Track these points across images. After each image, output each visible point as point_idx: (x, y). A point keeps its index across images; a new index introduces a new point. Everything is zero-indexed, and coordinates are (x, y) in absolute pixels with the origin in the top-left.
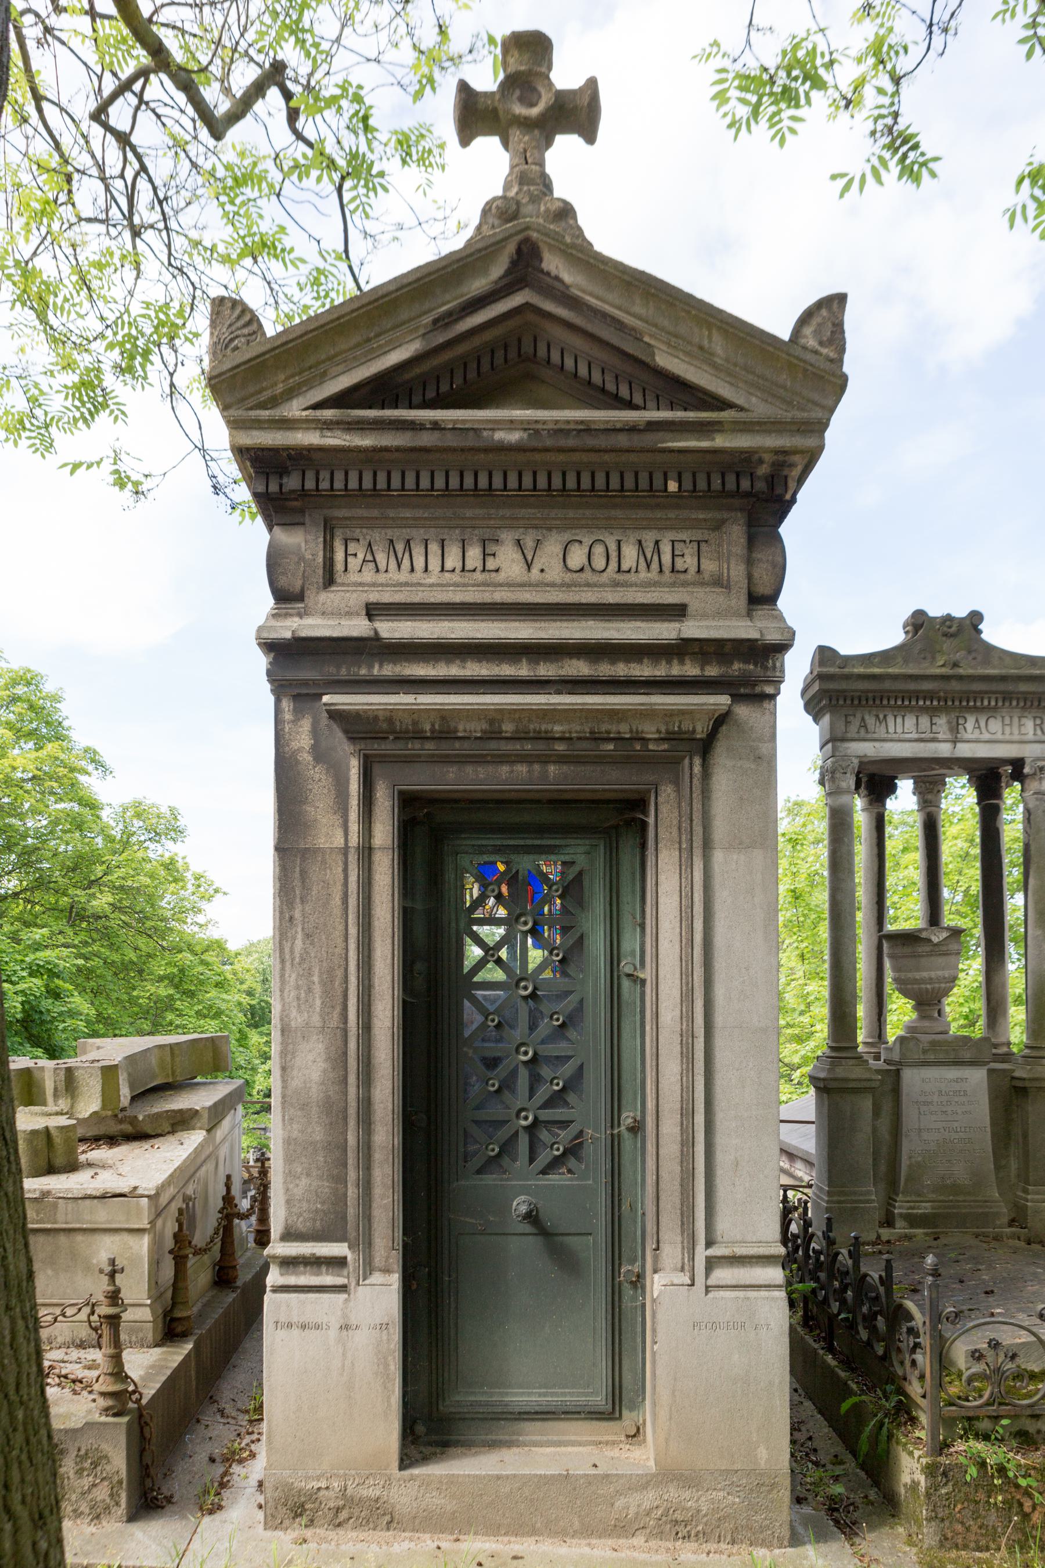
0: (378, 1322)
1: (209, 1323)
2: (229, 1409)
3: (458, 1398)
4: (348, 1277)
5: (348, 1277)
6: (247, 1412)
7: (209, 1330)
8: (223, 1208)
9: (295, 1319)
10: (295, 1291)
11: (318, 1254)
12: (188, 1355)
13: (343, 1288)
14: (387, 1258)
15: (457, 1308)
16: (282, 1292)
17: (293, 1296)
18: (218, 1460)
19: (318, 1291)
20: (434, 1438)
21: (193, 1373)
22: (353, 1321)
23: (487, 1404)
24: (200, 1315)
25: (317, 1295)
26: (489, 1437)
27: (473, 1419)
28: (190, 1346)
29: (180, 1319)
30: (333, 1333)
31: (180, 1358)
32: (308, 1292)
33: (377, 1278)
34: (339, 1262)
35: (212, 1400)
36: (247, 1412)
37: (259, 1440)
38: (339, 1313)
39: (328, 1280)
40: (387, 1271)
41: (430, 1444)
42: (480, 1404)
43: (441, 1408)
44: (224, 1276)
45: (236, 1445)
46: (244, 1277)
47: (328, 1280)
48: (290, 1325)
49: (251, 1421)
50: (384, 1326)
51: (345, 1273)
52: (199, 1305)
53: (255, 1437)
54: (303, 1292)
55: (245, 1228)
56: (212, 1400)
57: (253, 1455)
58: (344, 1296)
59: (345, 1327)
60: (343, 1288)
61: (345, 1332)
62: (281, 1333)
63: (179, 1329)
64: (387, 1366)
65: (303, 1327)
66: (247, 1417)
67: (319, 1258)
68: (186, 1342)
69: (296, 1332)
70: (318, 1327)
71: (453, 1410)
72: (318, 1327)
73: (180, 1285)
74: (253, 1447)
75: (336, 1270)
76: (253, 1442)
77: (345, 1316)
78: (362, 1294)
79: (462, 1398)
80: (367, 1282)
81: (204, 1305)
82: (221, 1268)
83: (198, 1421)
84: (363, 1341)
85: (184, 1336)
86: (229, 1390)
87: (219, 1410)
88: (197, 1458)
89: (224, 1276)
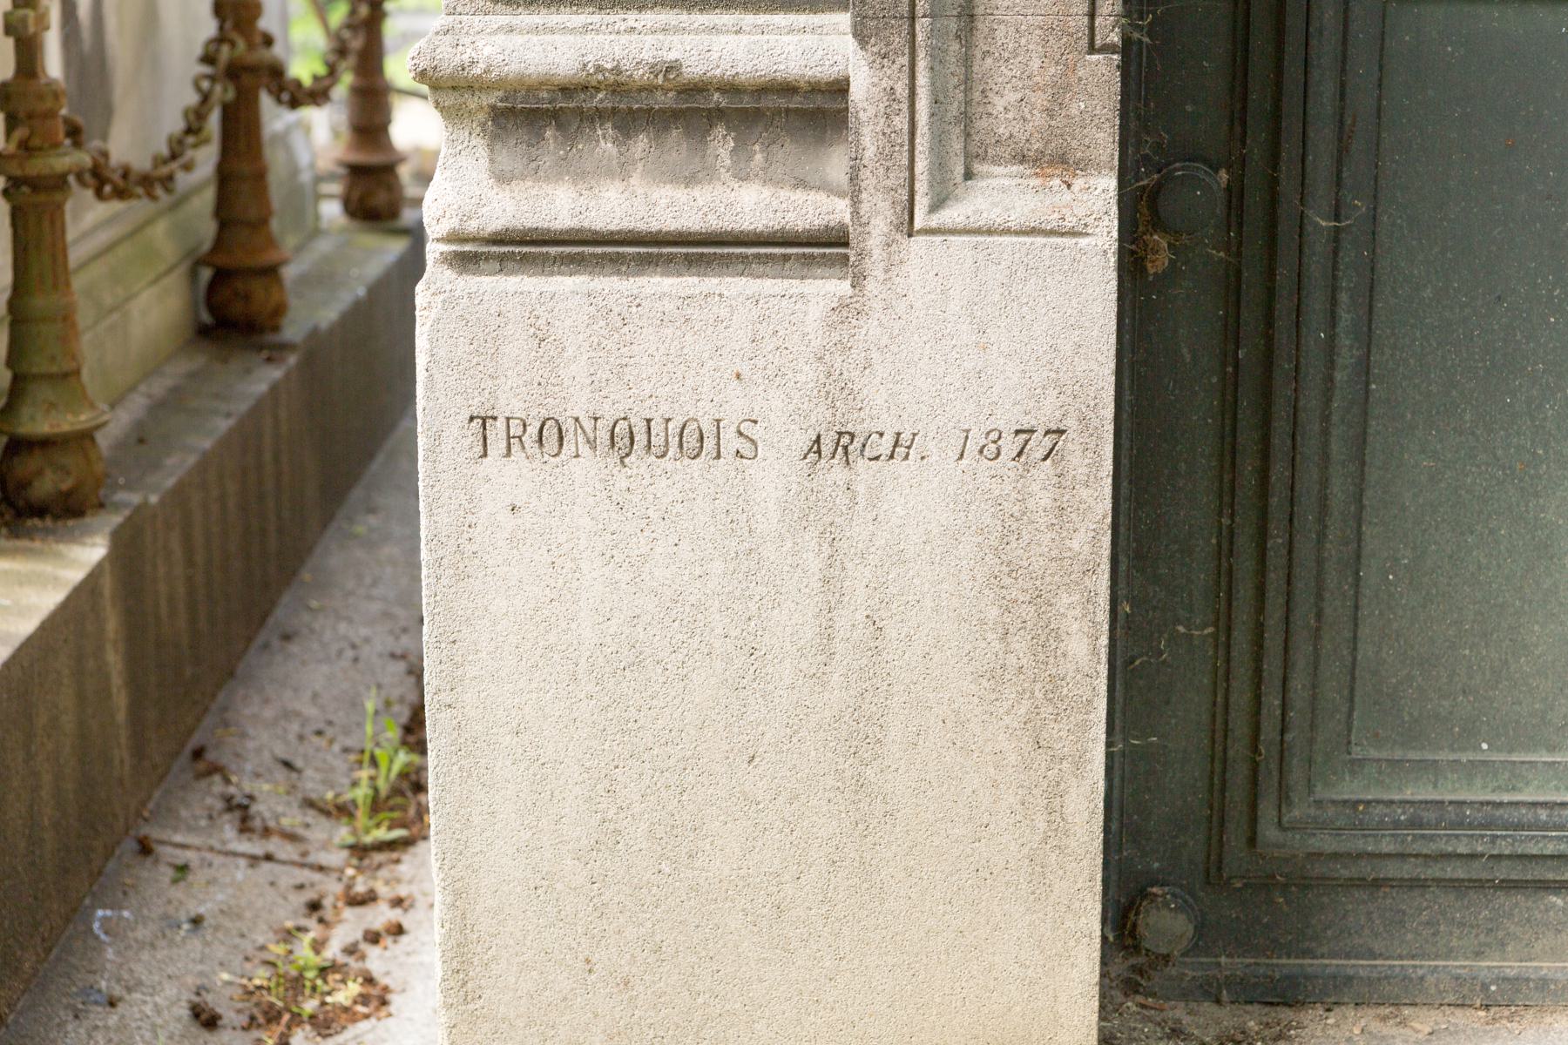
0: (1007, 420)
1: (176, 467)
2: (272, 803)
3: (1350, 789)
4: (854, 193)
5: (854, 193)
6: (344, 811)
7: (178, 495)
8: (221, 39)
9: (578, 405)
10: (577, 263)
11: (694, 69)
12: (87, 590)
13: (827, 247)
14: (1059, 93)
15: (1364, 368)
16: (504, 264)
17: (568, 285)
18: (229, 1016)
19: (695, 264)
20: (1231, 964)
21: (114, 660)
22: (879, 411)
23: (1491, 818)
24: (140, 437)
25: (690, 283)
26: (1488, 965)
27: (1416, 884)
28: (88, 553)
29: (46, 443)
30: (774, 476)
31: (48, 600)
32: (646, 264)
33: (1003, 194)
34: (813, 111)
35: (204, 764)
36: (344, 811)
37: (398, 930)
38: (808, 374)
39: (748, 200)
40: (1055, 160)
41: (1210, 992)
42: (1456, 816)
43: (1269, 832)
44: (231, 304)
45: (303, 951)
46: (311, 313)
47: (748, 200)
48: (551, 434)
49: (360, 851)
50: (1040, 442)
51: (836, 165)
52: (136, 406)
53: (380, 915)
54: (616, 264)
55: (315, 137)
56: (204, 764)
57: (377, 998)
58: (829, 288)
59: (838, 445)
60: (827, 247)
61: (837, 473)
62: (511, 476)
63: (47, 485)
64: (1048, 639)
65: (623, 441)
66: (343, 834)
67: (697, 89)
68: (73, 538)
69: (585, 468)
70: (694, 442)
71: (1325, 842)
72: (694, 442)
73: (39, 302)
74: (376, 960)
75: (787, 152)
76: (373, 938)
77: (836, 388)
78: (925, 281)
79: (1373, 787)
80: (951, 215)
81: (159, 407)
82: (222, 276)
83: (145, 849)
84: (922, 509)
85: (68, 510)
86: (295, 707)
87: (230, 805)
88: (138, 1007)
89: (231, 304)
